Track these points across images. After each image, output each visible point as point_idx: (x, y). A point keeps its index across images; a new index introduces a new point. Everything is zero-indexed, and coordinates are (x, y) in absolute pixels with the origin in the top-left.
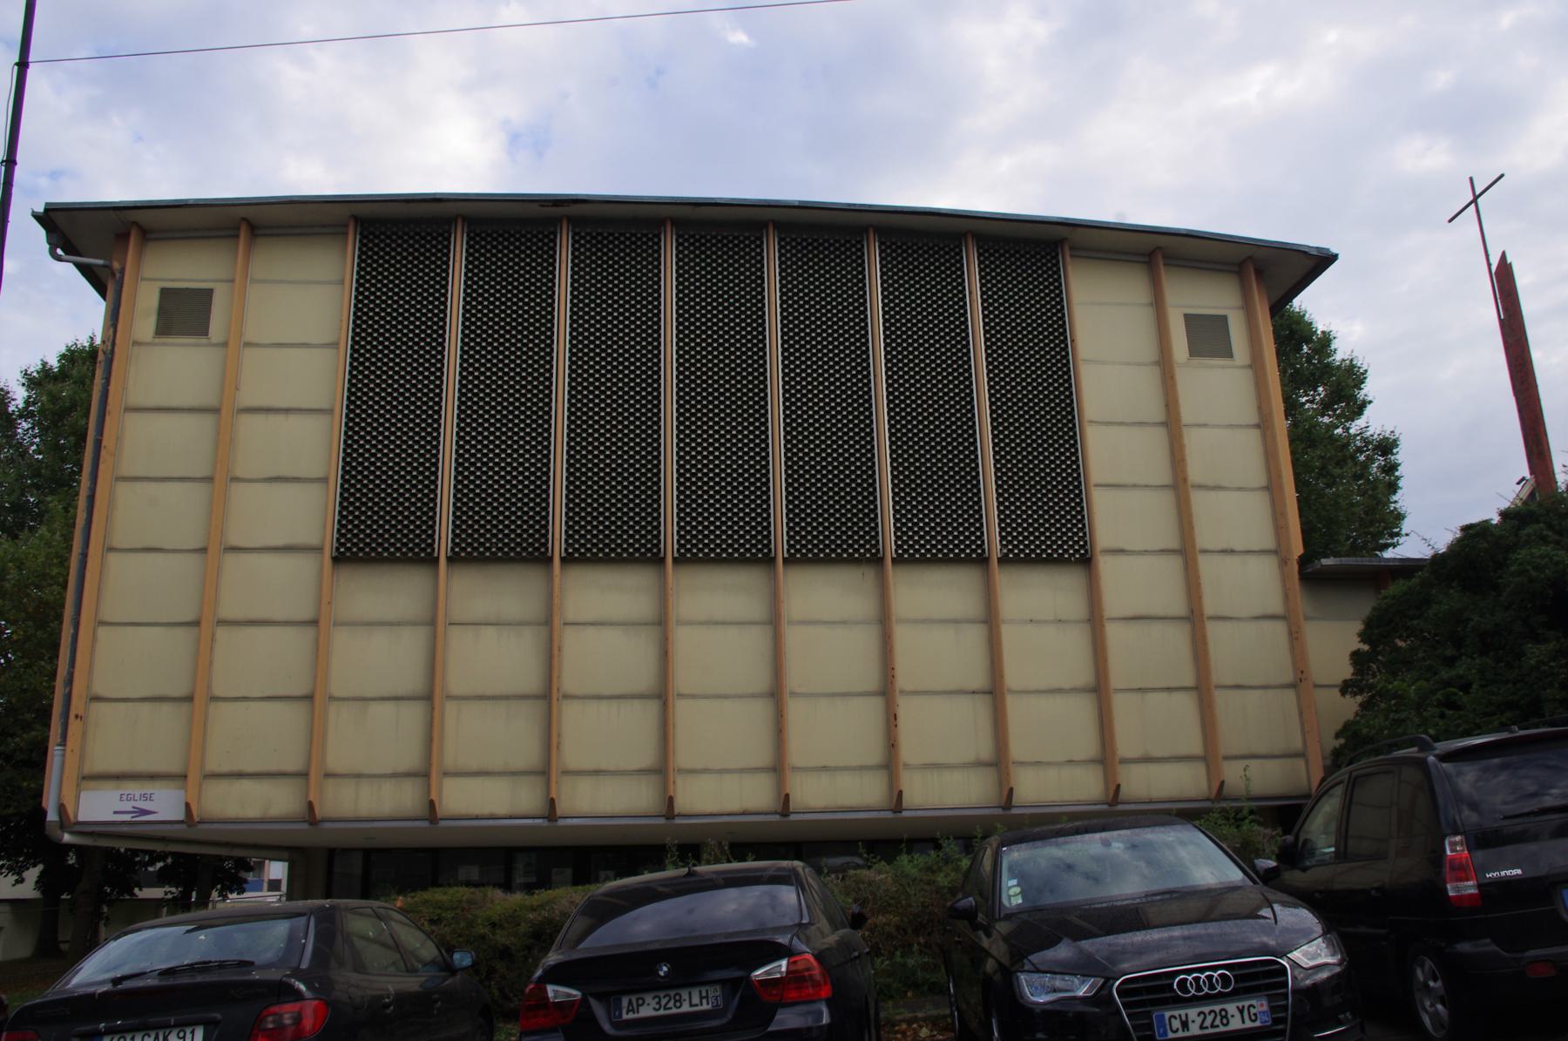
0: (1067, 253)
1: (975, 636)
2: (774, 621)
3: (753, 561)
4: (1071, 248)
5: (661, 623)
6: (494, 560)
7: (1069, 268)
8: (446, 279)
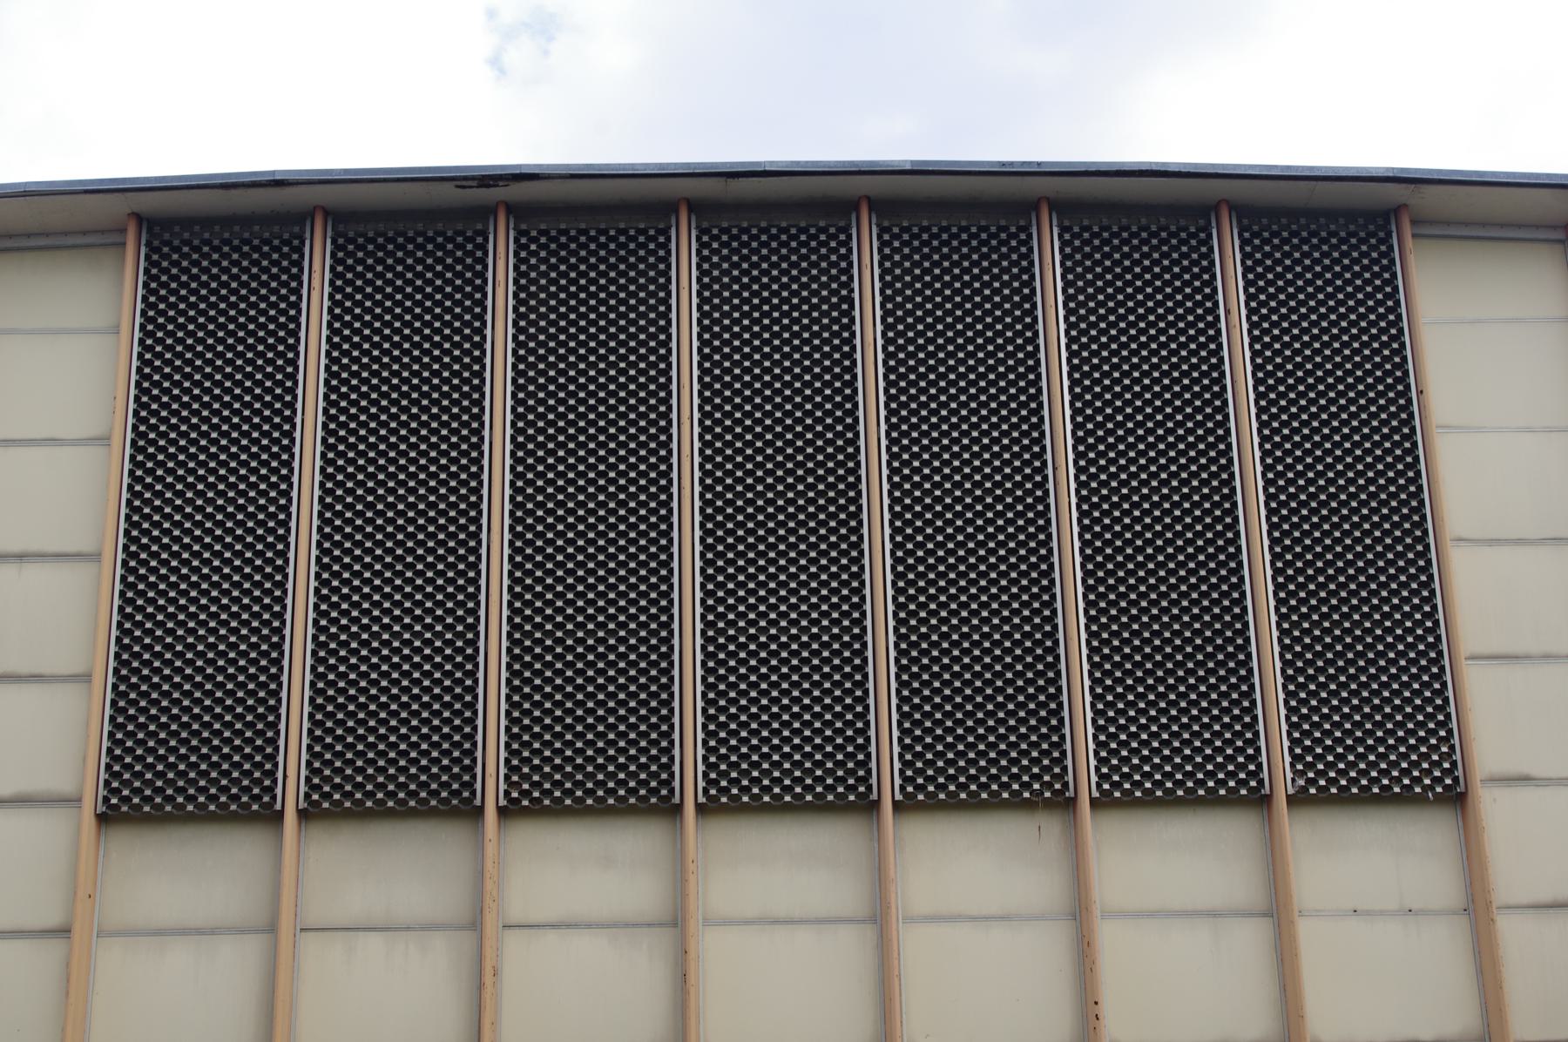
0: (1408, 231)
1: (1248, 942)
2: (879, 918)
3: (840, 808)
4: (1414, 222)
5: (676, 922)
6: (381, 813)
7: (1412, 260)
8: (296, 320)
